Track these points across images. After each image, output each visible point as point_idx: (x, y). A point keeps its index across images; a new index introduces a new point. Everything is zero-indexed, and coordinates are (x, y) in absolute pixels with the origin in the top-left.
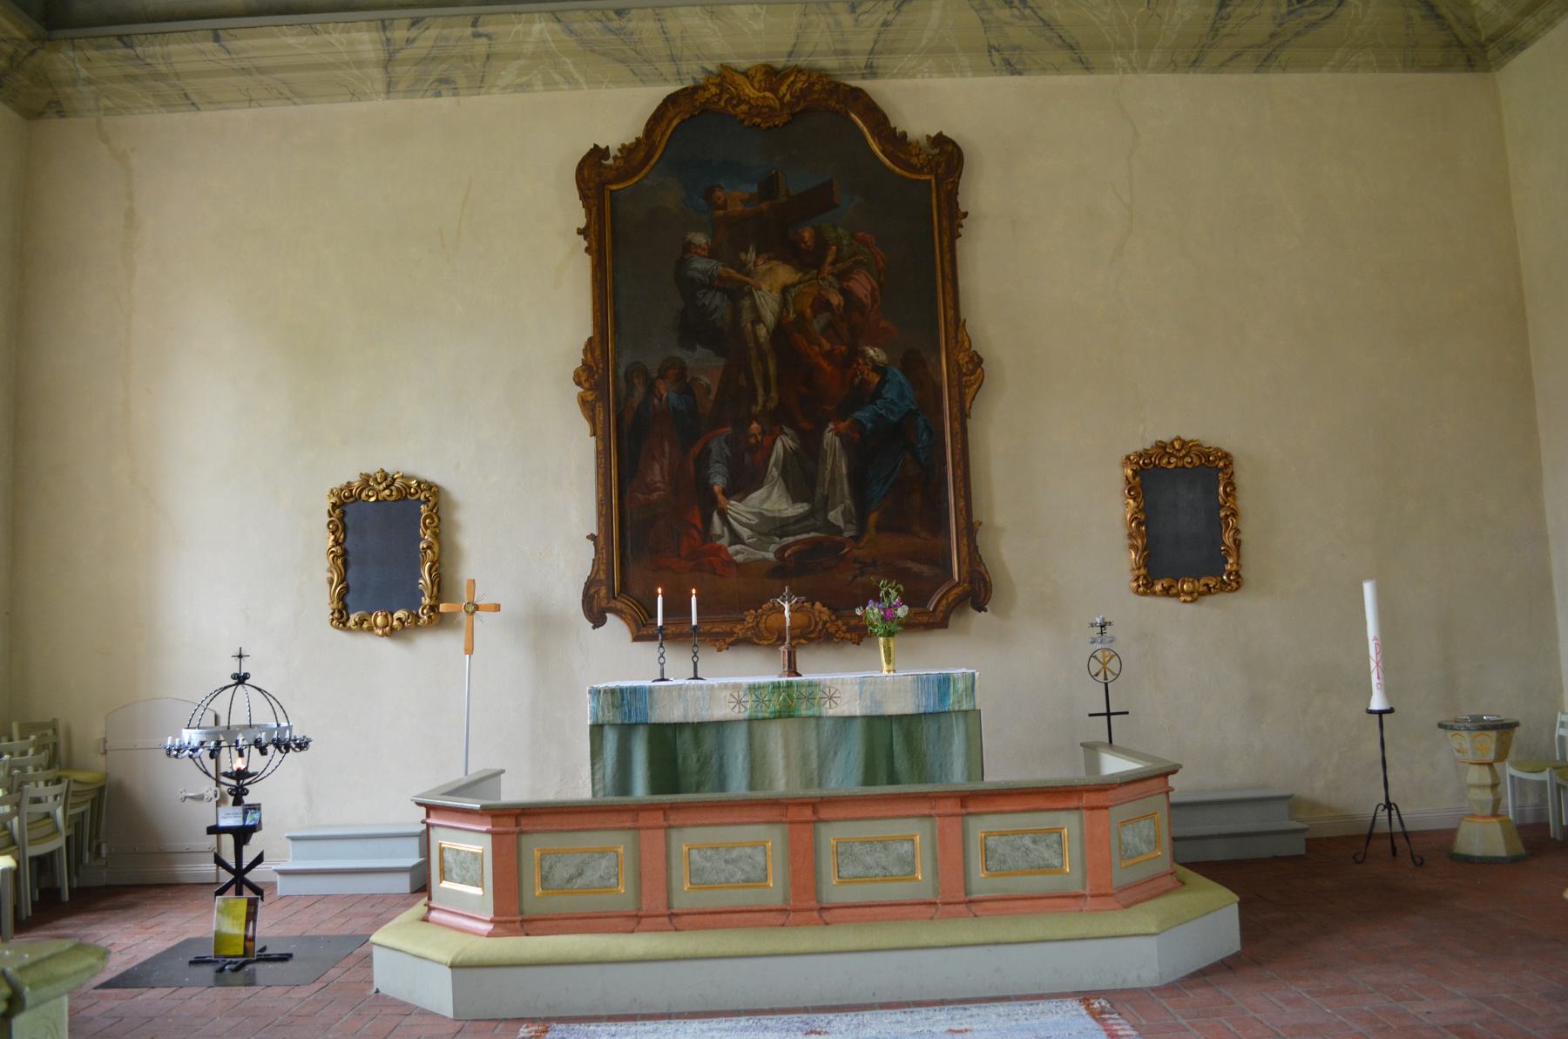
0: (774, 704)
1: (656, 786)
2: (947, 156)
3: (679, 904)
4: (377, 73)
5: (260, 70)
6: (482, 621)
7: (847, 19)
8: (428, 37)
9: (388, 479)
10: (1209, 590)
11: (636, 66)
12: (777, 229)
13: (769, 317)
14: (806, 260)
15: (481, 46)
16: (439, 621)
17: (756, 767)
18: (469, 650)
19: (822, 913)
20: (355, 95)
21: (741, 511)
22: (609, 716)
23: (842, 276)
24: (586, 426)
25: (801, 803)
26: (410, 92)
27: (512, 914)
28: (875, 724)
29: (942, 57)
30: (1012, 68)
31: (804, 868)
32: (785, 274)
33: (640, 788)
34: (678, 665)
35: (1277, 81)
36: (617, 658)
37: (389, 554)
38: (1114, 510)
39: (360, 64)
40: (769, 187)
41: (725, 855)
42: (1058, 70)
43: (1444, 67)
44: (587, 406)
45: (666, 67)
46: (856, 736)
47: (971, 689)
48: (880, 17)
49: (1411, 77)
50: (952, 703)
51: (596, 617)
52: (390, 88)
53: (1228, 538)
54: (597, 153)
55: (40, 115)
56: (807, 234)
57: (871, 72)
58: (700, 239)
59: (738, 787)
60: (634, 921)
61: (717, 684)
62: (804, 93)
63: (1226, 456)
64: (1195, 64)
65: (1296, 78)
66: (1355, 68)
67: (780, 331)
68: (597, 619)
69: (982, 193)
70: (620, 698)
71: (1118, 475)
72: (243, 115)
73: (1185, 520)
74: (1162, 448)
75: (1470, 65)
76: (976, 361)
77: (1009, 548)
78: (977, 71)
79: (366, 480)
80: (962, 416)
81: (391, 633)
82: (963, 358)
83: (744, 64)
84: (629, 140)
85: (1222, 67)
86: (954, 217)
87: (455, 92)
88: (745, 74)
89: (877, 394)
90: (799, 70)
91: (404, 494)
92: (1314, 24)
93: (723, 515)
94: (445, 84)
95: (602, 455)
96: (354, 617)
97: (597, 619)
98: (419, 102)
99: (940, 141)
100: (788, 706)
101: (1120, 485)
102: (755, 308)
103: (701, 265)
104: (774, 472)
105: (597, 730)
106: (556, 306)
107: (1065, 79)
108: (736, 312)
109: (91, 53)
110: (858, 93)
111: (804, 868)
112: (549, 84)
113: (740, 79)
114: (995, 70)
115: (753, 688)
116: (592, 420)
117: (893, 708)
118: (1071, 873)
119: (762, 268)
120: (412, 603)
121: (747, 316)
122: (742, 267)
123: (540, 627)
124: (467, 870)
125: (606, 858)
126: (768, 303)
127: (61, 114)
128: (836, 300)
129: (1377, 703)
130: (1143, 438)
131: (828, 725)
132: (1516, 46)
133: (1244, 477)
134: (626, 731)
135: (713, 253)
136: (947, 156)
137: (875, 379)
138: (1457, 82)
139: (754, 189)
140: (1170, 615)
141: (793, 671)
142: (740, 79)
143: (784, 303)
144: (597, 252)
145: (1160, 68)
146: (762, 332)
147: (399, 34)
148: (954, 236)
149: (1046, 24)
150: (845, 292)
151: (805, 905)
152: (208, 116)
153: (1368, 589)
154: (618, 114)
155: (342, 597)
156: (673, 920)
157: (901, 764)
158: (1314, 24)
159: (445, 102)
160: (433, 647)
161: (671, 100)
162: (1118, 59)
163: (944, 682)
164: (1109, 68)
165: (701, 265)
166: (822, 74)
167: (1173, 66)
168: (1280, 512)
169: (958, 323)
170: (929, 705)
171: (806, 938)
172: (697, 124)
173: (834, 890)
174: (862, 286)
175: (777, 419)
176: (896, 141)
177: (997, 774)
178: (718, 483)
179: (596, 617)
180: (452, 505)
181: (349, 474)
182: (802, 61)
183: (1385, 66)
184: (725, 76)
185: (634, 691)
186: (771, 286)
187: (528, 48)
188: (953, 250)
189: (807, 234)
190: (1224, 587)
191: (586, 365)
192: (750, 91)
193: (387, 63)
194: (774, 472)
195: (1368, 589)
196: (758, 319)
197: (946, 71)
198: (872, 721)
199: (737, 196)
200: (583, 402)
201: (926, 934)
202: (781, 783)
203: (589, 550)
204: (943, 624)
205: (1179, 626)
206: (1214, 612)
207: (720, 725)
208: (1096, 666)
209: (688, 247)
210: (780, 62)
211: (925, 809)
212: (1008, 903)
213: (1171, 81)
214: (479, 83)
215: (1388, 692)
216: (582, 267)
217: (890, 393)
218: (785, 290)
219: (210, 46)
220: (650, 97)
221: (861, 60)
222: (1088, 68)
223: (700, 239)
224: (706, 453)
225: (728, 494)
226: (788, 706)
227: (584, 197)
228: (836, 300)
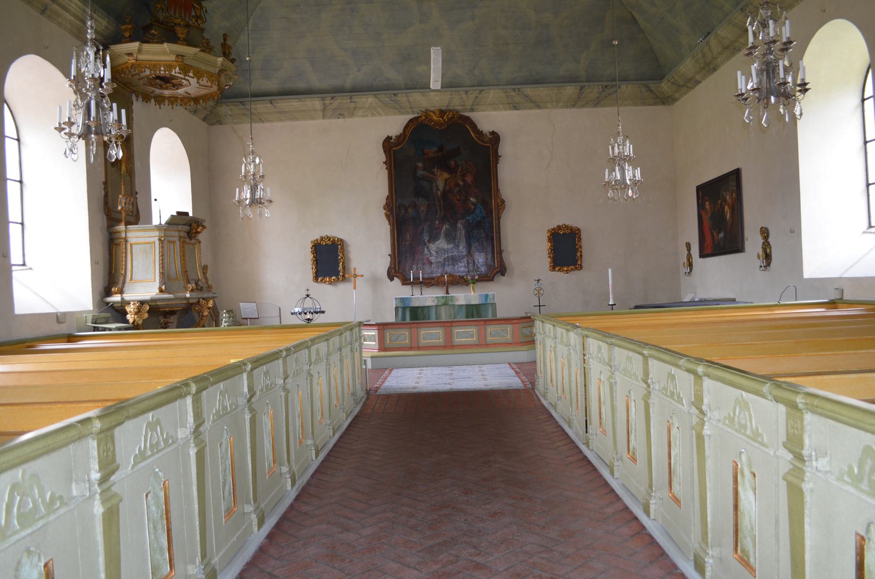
0: (443, 301)
1: (412, 319)
2: (495, 138)
3: (420, 345)
4: (321, 113)
5: (284, 112)
6: (359, 280)
7: (464, 96)
8: (336, 103)
9: (329, 238)
10: (572, 270)
11: (400, 110)
12: (443, 162)
13: (441, 189)
14: (451, 171)
15: (353, 105)
16: (344, 279)
17: (438, 316)
18: (355, 288)
19: (453, 347)
20: (313, 119)
21: (433, 247)
22: (399, 305)
23: (463, 176)
24: (387, 222)
25: (448, 322)
26: (330, 118)
27: (382, 347)
28: (469, 307)
29: (494, 106)
30: (516, 108)
31: (449, 336)
32: (446, 175)
33: (408, 320)
34: (417, 291)
35: (599, 110)
36: (397, 290)
37: (329, 260)
38: (545, 246)
39: (315, 110)
40: (441, 148)
41: (431, 335)
42: (531, 108)
43: (655, 104)
44: (387, 216)
45: (409, 110)
46: (464, 309)
47: (494, 298)
48: (474, 96)
49: (644, 108)
50: (489, 301)
51: (391, 278)
52: (324, 117)
53: (578, 254)
54: (389, 138)
55: (214, 124)
56: (452, 163)
57: (472, 110)
58: (420, 165)
59: (433, 319)
60: (411, 349)
61: (428, 297)
62: (452, 118)
63: (579, 230)
64: (574, 106)
65: (607, 109)
66: (626, 105)
67: (444, 193)
68: (392, 279)
69: (505, 149)
70: (403, 300)
71: (546, 235)
72: (279, 124)
73: (565, 249)
74: (559, 227)
75: (663, 103)
76: (503, 202)
77: (512, 257)
78: (505, 109)
79: (322, 238)
80: (499, 218)
81: (330, 283)
82: (499, 201)
83: (433, 109)
84: (398, 134)
85: (582, 106)
86: (497, 157)
87: (344, 117)
88: (433, 112)
89: (474, 212)
90: (450, 111)
91: (334, 243)
92: (611, 94)
93: (428, 248)
94: (341, 115)
95: (392, 231)
96: (320, 279)
97: (392, 279)
98: (332, 120)
99: (493, 133)
100: (446, 302)
101: (547, 239)
102: (437, 186)
103: (420, 173)
104: (442, 235)
105: (397, 308)
106: (377, 185)
107: (533, 111)
108: (431, 188)
109: (232, 107)
110: (468, 118)
111: (449, 336)
112: (373, 115)
113: (432, 114)
114: (510, 109)
115: (437, 298)
116: (389, 220)
117: (473, 302)
118: (509, 337)
119: (439, 173)
120: (337, 275)
121: (434, 188)
122: (433, 173)
123: (374, 280)
124: (371, 338)
125: (403, 336)
126: (441, 184)
127: (221, 124)
128: (461, 183)
129: (611, 303)
130: (553, 225)
131: (456, 308)
132: (698, 82)
133: (584, 236)
134: (404, 308)
135: (424, 169)
136: (495, 138)
137: (473, 207)
138: (659, 108)
139: (436, 149)
140: (560, 277)
141: (447, 293)
142: (432, 114)
143: (446, 184)
144: (389, 169)
145: (563, 107)
146: (439, 193)
147: (328, 101)
148: (497, 163)
149: (526, 96)
150: (464, 181)
151: (449, 345)
152: (267, 125)
153: (610, 270)
154: (394, 125)
155: (316, 273)
156: (419, 348)
157: (475, 313)
158: (611, 94)
159: (341, 120)
160: (342, 287)
161: (411, 121)
162: (549, 105)
163: (487, 296)
164: (547, 108)
165: (420, 173)
166: (457, 112)
167: (567, 107)
168: (591, 247)
169: (498, 190)
170: (483, 302)
171: (449, 351)
172: (418, 129)
173: (457, 340)
174: (469, 179)
175: (444, 220)
176: (480, 133)
177: (499, 316)
178: (426, 238)
179: (391, 278)
180: (348, 246)
181: (317, 236)
182: (451, 108)
183: (635, 104)
184: (427, 113)
185: (406, 298)
186: (441, 179)
187: (367, 106)
188: (496, 167)
189: (452, 163)
190: (576, 269)
191: (387, 204)
192: (435, 118)
193: (324, 110)
194: (442, 235)
195: (610, 270)
196: (438, 189)
197: (495, 110)
198: (467, 305)
199: (431, 151)
200: (386, 215)
201: (475, 351)
202: (444, 319)
203: (389, 259)
204: (492, 280)
205: (563, 279)
206: (574, 275)
207: (428, 307)
208: (536, 292)
209: (416, 167)
210: (444, 108)
211: (476, 323)
212: (495, 345)
213: (566, 111)
214: (352, 115)
215: (614, 299)
216: (385, 173)
217: (477, 211)
218: (446, 180)
219: (269, 105)
220: (404, 119)
221: (469, 107)
222: (539, 107)
223: (420, 165)
224: (423, 230)
225: (429, 242)
226: (446, 302)
227: (385, 152)
228: (461, 183)
